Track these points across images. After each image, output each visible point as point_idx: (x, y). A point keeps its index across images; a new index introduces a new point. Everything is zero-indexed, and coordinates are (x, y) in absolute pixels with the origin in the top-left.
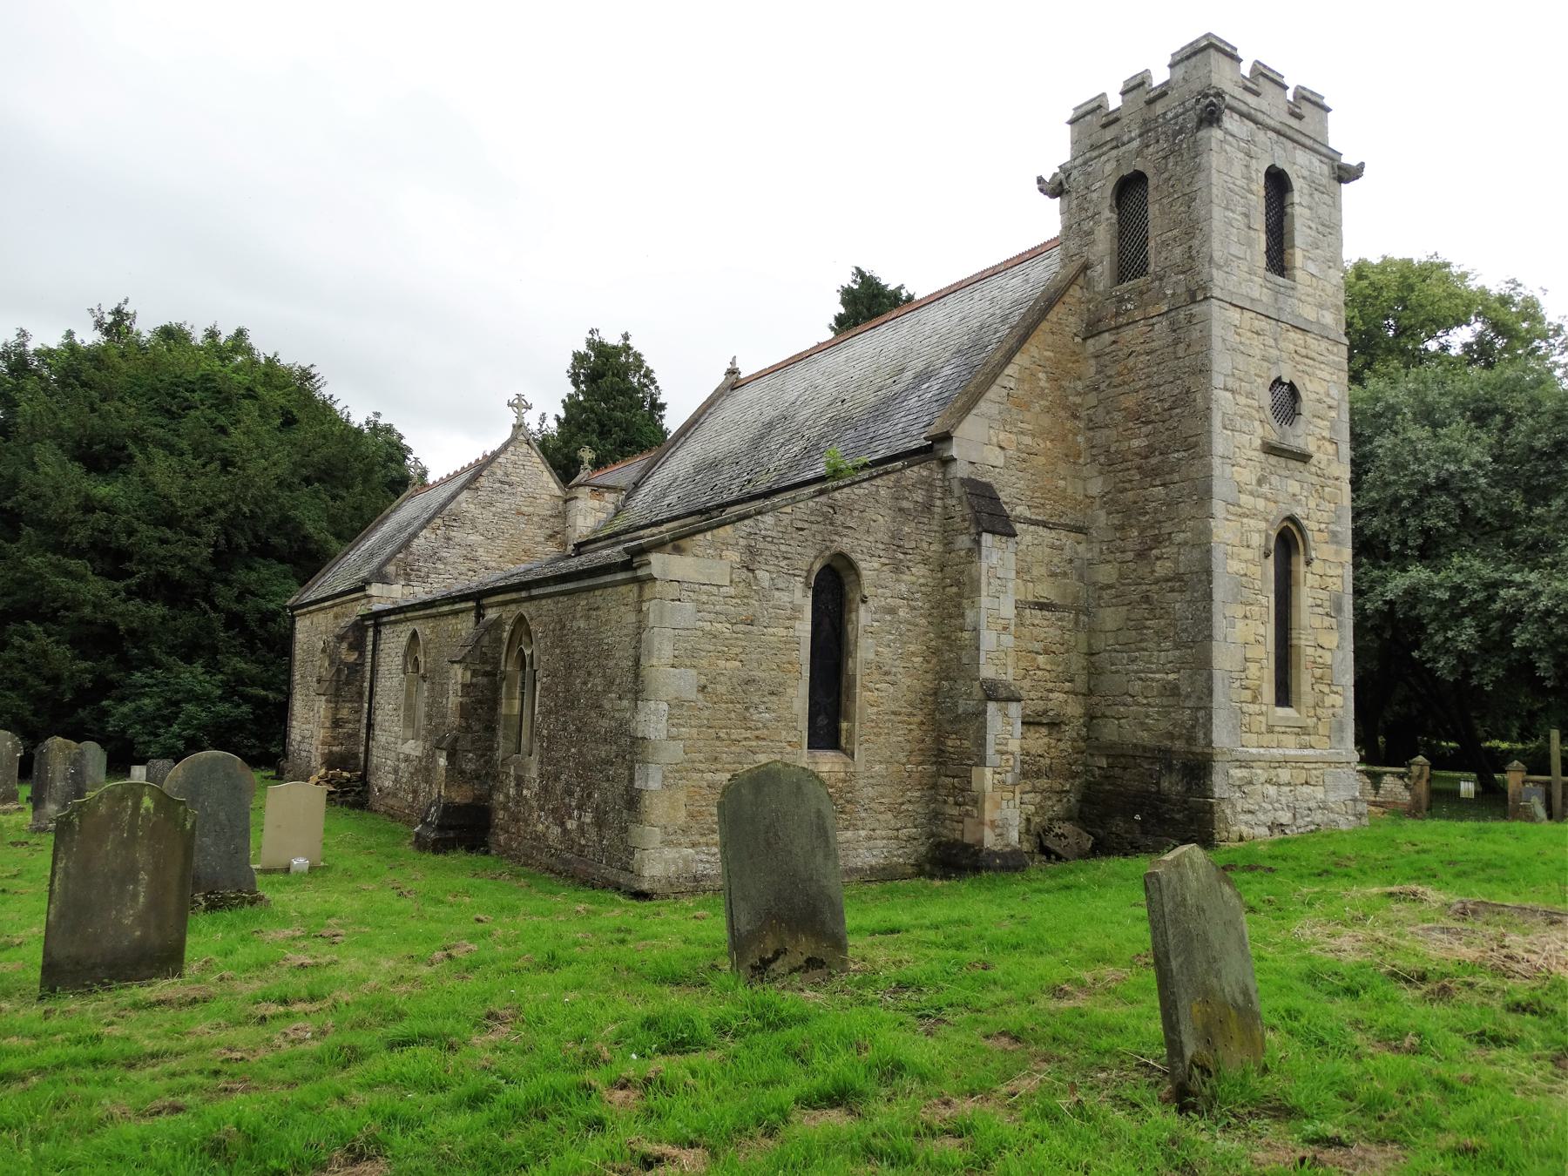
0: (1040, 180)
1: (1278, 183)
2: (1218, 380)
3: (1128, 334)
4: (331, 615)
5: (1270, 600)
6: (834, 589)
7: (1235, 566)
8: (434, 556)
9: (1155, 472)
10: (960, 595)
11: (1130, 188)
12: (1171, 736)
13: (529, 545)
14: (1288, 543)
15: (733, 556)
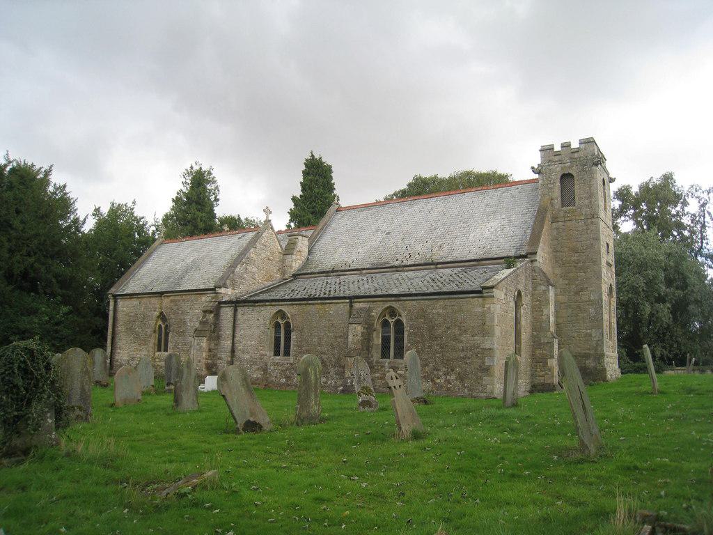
0: (533, 168)
3: (568, 224)
8: (242, 277)
9: (581, 268)
11: (567, 177)
12: (589, 349)
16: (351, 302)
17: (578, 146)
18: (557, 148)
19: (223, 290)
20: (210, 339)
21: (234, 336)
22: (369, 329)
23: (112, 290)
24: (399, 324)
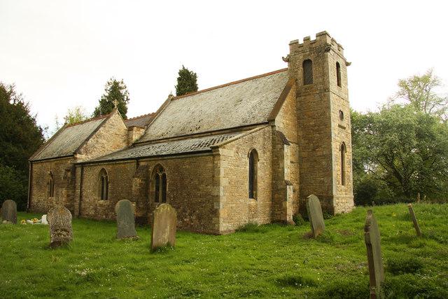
1: (338, 65)
2: (332, 110)
3: (308, 97)
4: (53, 164)
5: (340, 161)
6: (253, 156)
7: (335, 153)
9: (317, 131)
10: (278, 160)
11: (307, 63)
13: (118, 144)
14: (343, 148)
15: (234, 149)
16: (138, 162)
17: (315, 38)
18: (301, 42)
19: (78, 156)
20: (68, 188)
21: (81, 187)
22: (147, 180)
23: (31, 159)
24: (164, 176)
